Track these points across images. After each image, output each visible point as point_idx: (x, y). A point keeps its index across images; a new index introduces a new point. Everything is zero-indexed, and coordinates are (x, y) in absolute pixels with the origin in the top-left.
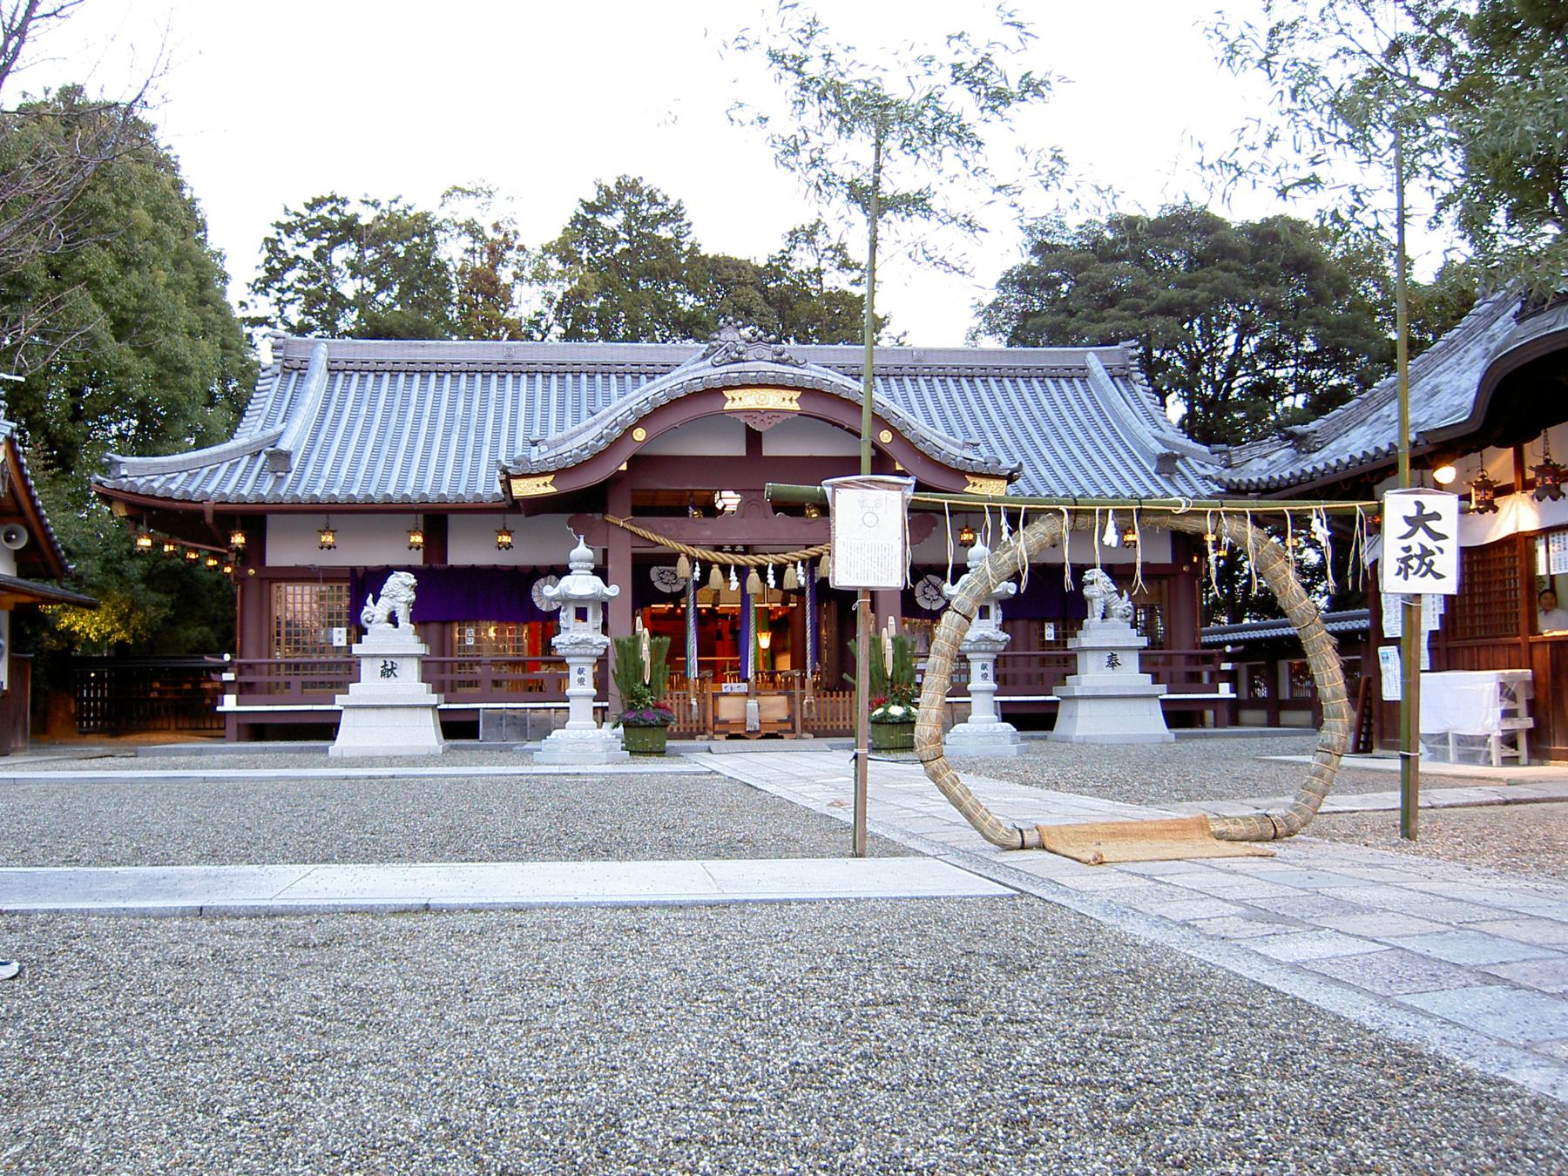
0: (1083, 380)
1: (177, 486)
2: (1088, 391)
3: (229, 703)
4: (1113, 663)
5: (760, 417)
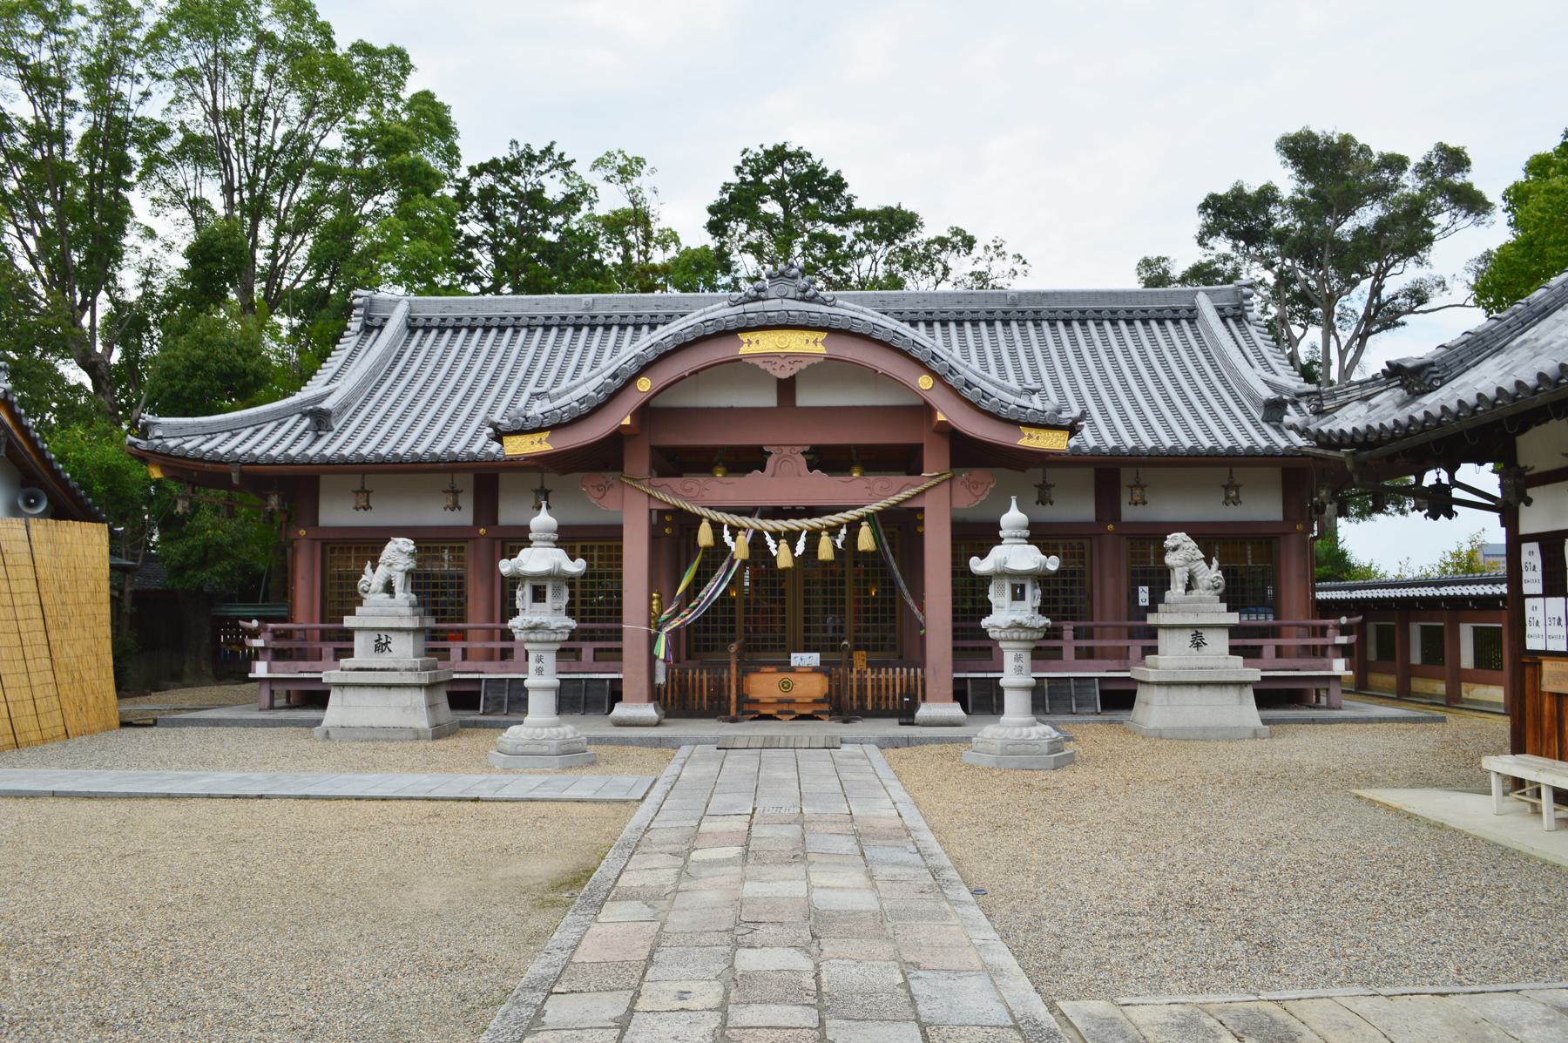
0: (1191, 321)
1: (223, 446)
2: (1198, 336)
3: (261, 669)
4: (1198, 643)
5: (780, 362)
